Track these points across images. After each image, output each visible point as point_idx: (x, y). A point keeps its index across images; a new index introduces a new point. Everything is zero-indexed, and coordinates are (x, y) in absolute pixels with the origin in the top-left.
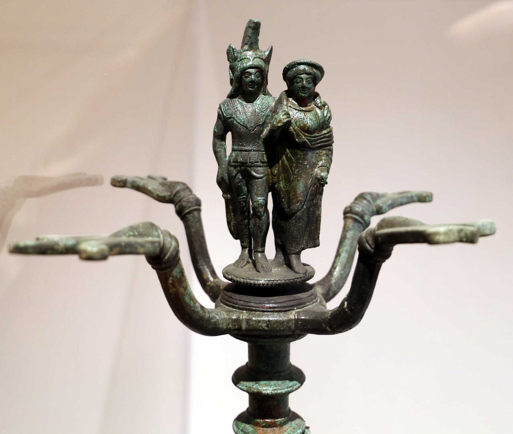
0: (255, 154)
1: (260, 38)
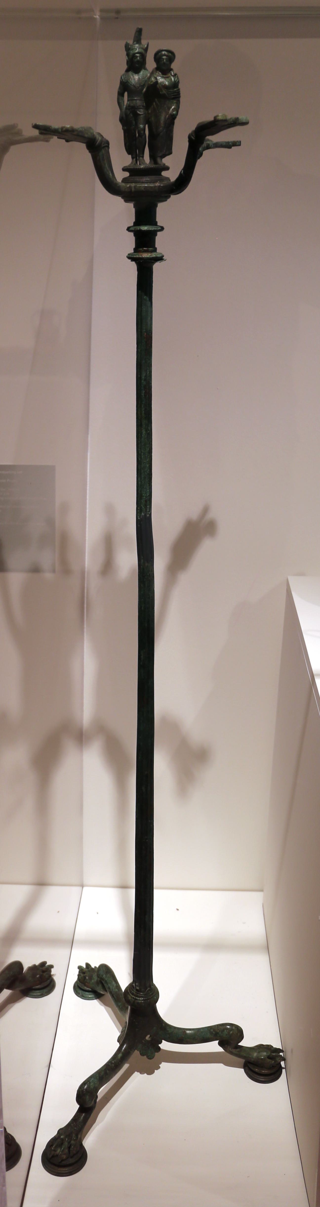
0: (138, 102)
1: (173, 197)
